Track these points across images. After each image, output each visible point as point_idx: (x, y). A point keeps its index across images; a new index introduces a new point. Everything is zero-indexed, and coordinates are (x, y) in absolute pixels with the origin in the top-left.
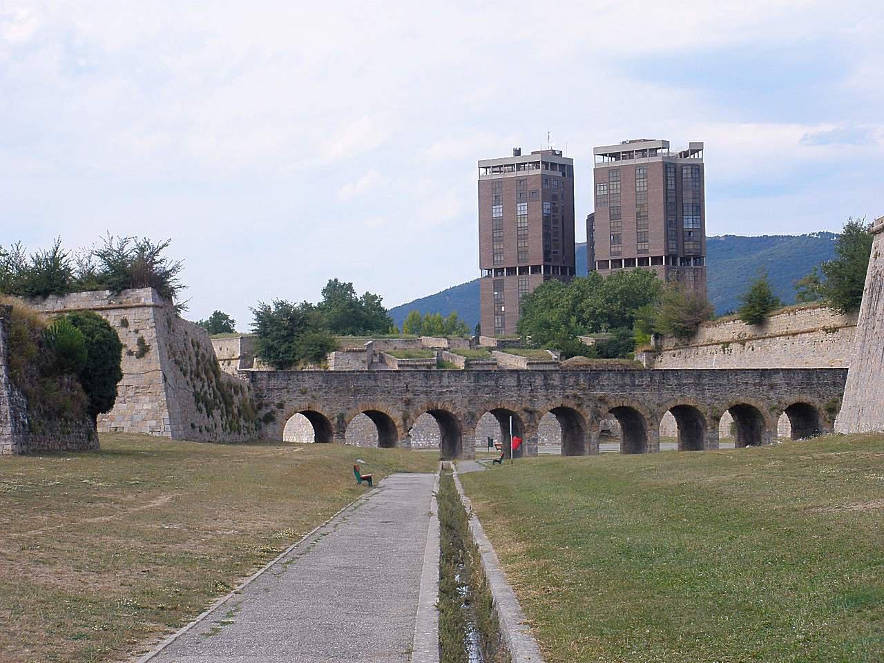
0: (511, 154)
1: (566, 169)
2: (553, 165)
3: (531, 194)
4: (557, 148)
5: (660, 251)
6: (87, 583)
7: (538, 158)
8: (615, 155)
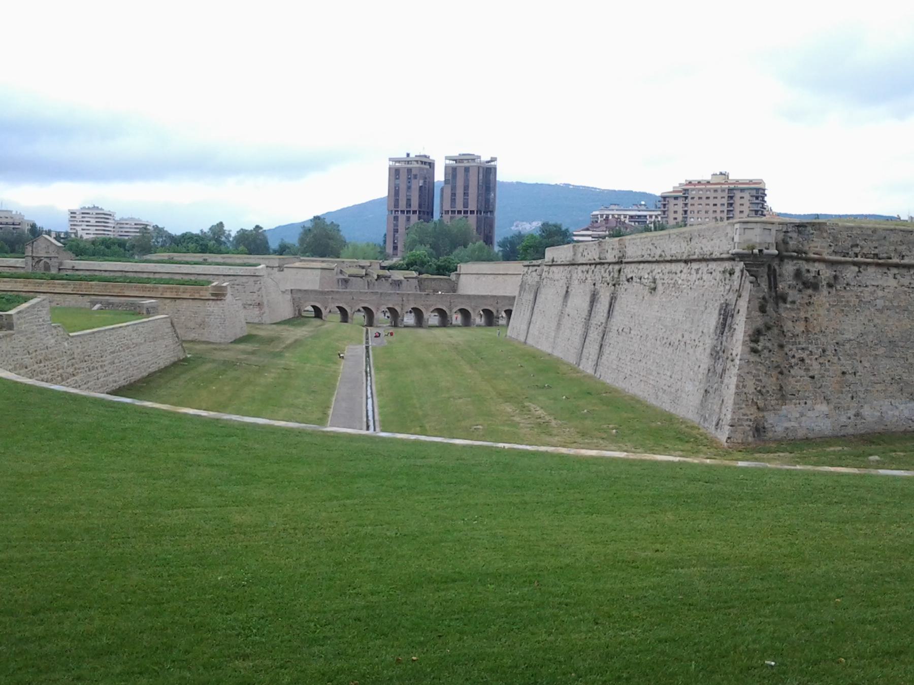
0: (405, 156)
1: (431, 165)
2: (425, 163)
3: (410, 177)
4: (427, 154)
5: (474, 209)
6: (521, 503)
7: (417, 159)
8: (456, 160)
